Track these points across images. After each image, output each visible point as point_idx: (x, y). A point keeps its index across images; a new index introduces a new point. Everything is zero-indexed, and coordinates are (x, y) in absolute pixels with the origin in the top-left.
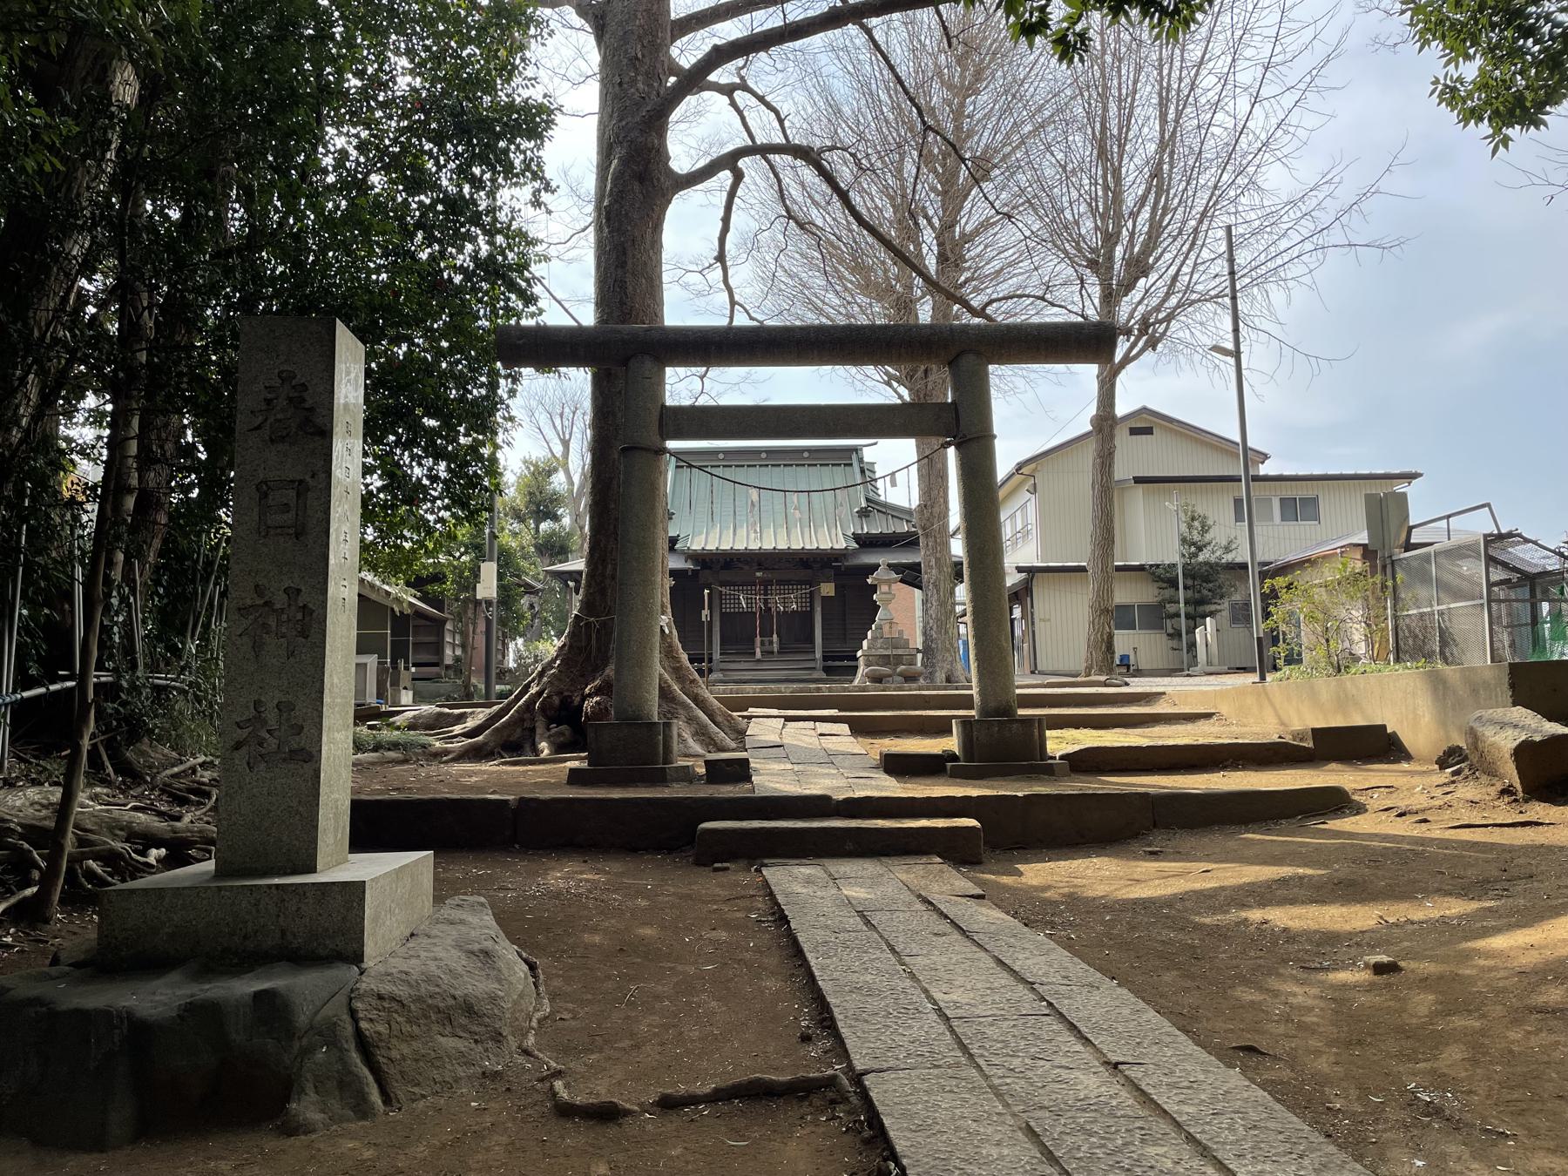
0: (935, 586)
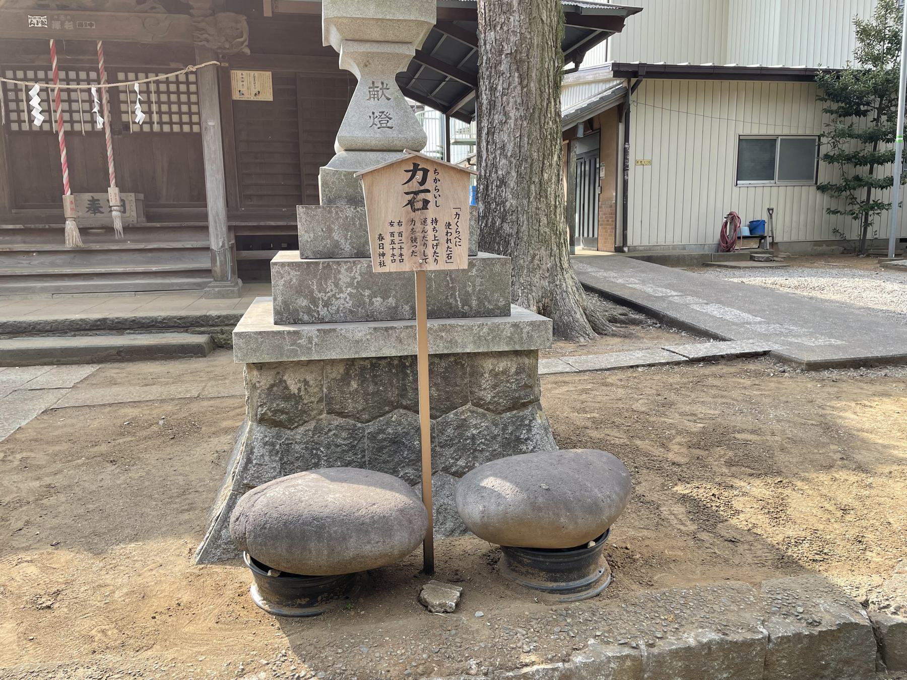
0: (518, 62)
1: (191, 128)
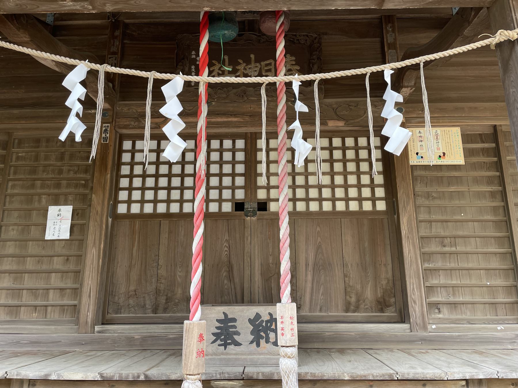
1: (374, 205)
